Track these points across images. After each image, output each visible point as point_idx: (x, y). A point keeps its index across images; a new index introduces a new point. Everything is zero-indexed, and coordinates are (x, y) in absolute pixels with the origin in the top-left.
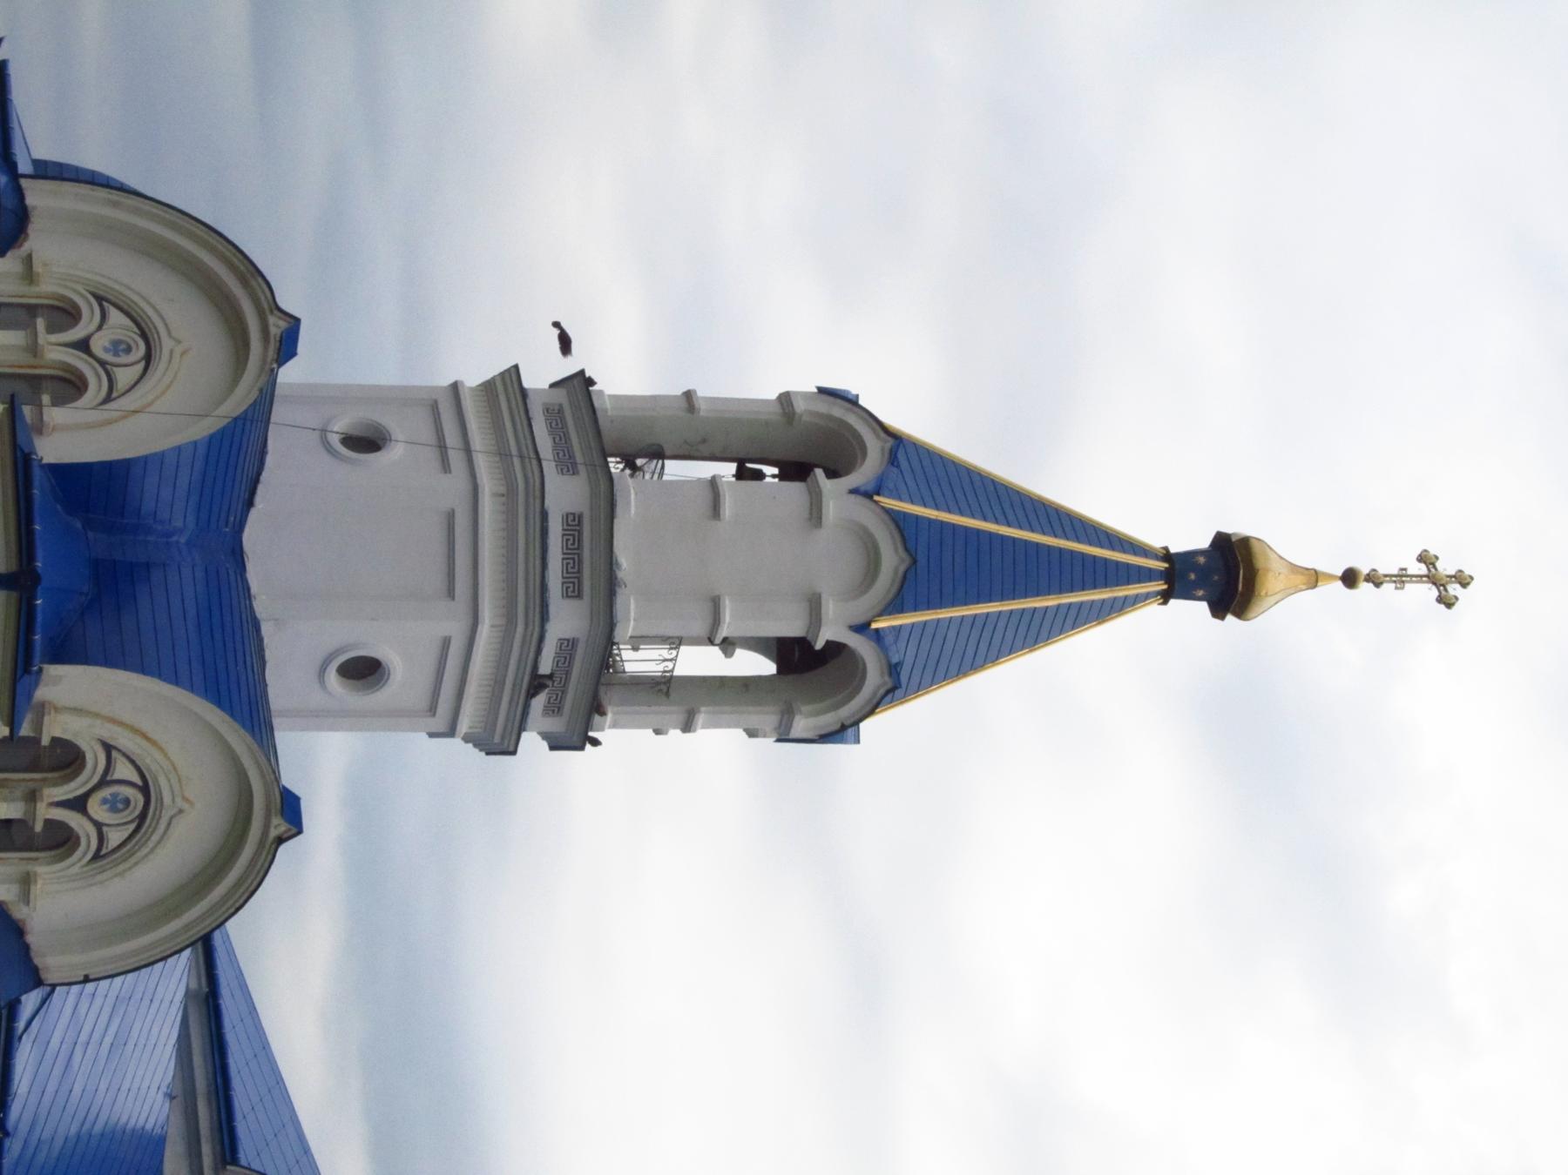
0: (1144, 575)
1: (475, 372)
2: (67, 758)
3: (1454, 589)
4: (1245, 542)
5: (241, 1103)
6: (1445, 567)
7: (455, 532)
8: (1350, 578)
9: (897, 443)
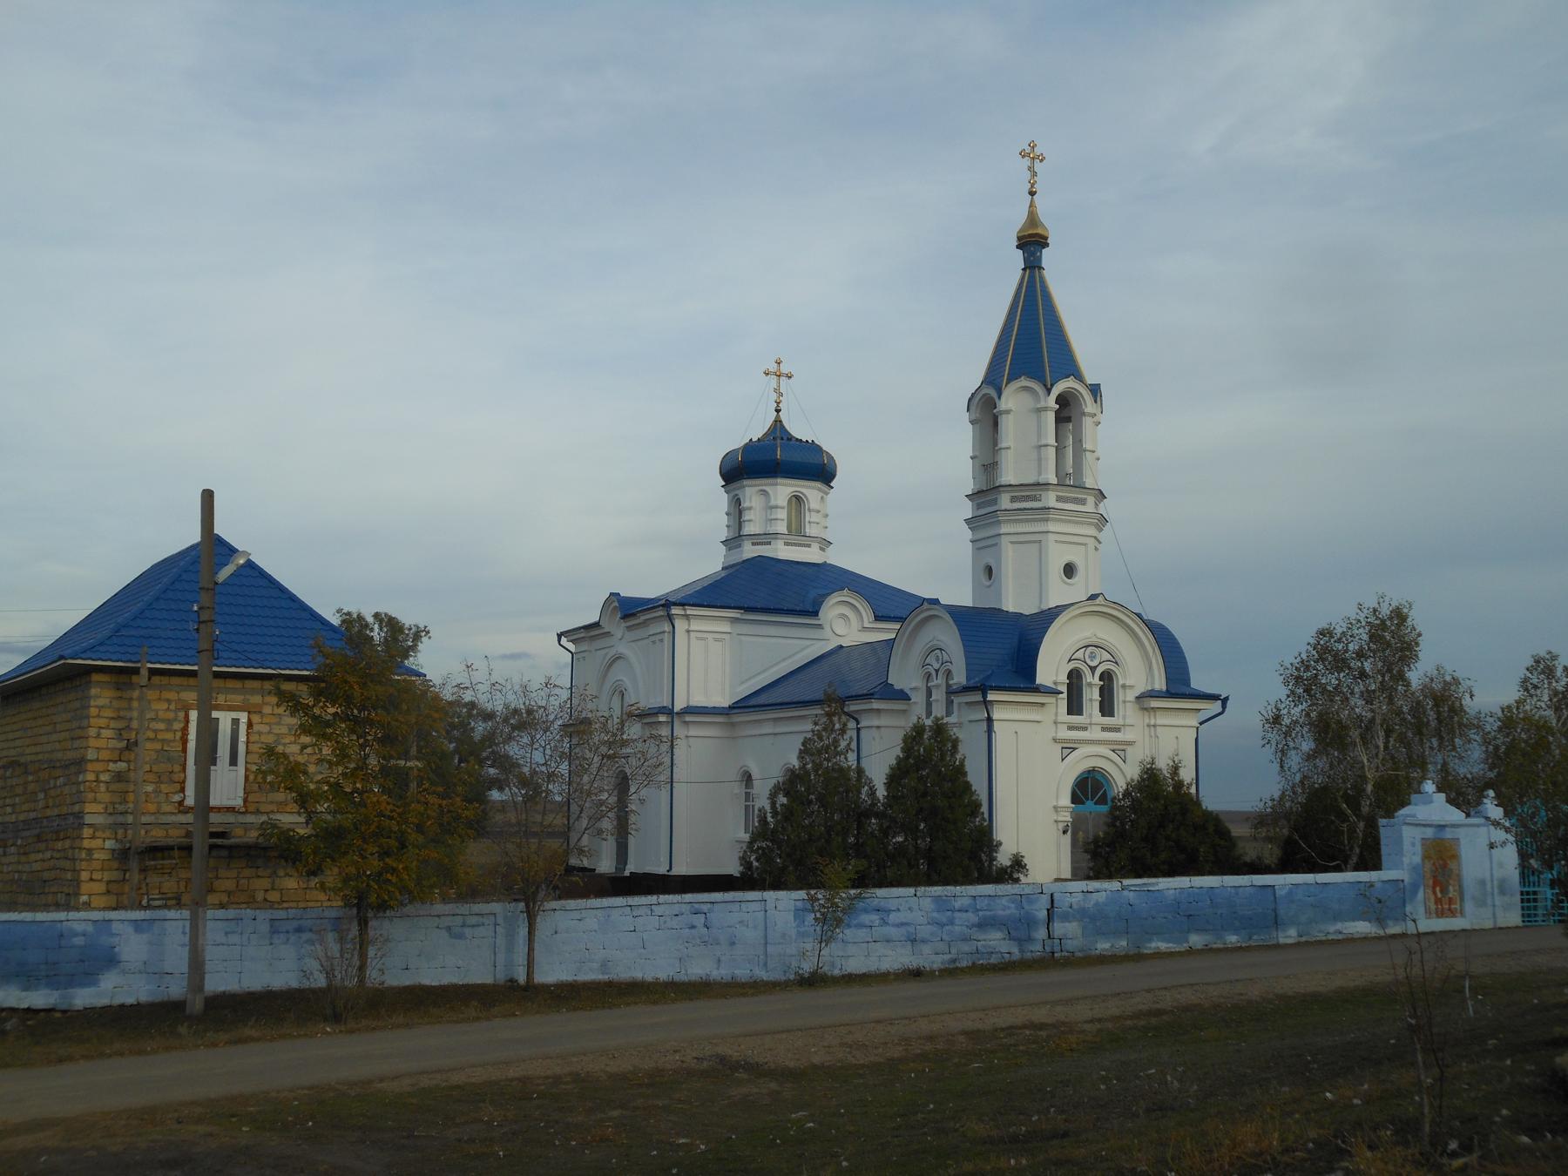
0: (1032, 277)
1: (968, 534)
3: (1028, 150)
4: (1019, 239)
5: (807, 698)
6: (773, 367)
8: (1032, 194)
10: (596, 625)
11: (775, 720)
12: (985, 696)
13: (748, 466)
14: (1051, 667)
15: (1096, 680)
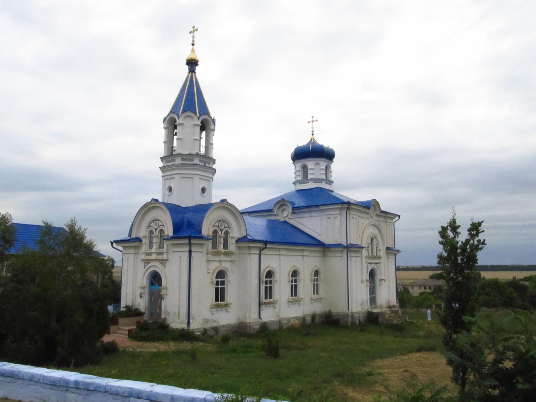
1: (160, 173)
2: (215, 232)
4: (187, 60)
7: (184, 177)
8: (193, 45)
9: (171, 112)
10: (270, 211)
11: (311, 250)
12: (190, 241)
13: (301, 155)
14: (206, 230)
15: (223, 235)
